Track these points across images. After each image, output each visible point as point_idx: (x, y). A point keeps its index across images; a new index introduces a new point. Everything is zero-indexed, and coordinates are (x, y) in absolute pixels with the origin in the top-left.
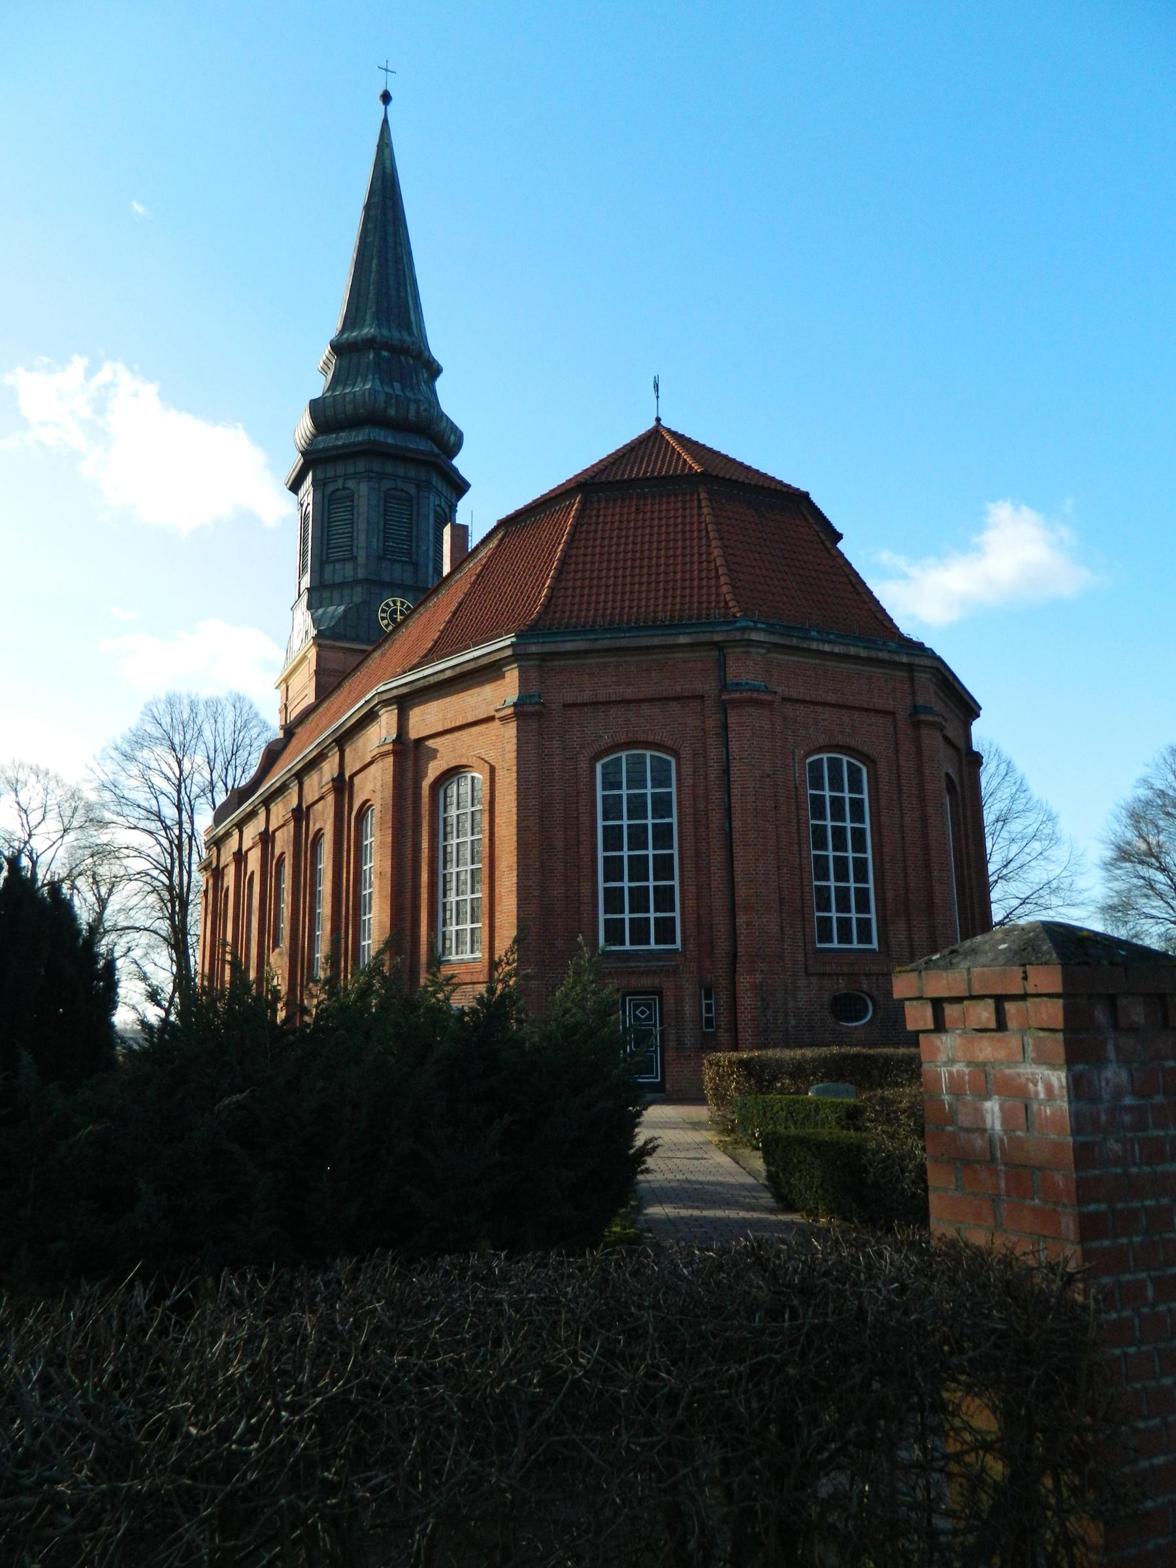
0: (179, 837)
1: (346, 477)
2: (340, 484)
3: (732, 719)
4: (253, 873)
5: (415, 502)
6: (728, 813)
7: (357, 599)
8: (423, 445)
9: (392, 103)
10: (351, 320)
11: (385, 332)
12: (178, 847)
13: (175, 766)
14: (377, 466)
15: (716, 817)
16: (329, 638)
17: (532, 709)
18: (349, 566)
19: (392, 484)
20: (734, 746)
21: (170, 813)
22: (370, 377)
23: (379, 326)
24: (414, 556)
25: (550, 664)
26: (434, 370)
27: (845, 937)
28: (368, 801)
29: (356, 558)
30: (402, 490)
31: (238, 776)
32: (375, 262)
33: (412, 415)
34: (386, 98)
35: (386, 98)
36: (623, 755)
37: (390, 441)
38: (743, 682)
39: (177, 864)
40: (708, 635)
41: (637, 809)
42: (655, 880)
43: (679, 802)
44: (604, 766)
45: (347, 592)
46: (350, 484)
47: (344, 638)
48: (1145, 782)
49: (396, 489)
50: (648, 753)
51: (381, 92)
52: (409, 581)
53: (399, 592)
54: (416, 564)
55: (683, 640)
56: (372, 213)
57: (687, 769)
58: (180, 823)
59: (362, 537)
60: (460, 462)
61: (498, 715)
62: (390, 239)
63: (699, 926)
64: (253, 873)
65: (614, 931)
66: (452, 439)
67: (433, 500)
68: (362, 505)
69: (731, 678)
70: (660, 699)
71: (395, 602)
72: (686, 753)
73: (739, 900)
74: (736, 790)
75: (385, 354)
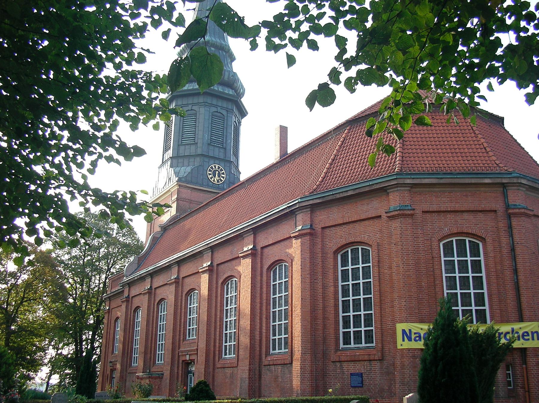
1: (193, 104)
2: (189, 108)
5: (226, 118)
6: (516, 271)
7: (197, 164)
8: (229, 92)
11: (213, 39)
14: (209, 100)
15: (508, 274)
16: (183, 182)
18: (193, 147)
19: (214, 109)
20: (517, 238)
24: (224, 145)
25: (413, 190)
26: (233, 59)
29: (197, 143)
36: (454, 239)
38: (518, 204)
40: (500, 179)
41: (357, 304)
43: (486, 265)
44: (341, 255)
45: (192, 160)
46: (194, 108)
47: (191, 183)
48: (440, 315)
52: (222, 157)
53: (217, 162)
54: (225, 149)
57: (490, 248)
59: (201, 133)
60: (245, 101)
65: (347, 341)
69: (511, 202)
70: (473, 211)
71: (215, 166)
72: (489, 240)
74: (519, 259)
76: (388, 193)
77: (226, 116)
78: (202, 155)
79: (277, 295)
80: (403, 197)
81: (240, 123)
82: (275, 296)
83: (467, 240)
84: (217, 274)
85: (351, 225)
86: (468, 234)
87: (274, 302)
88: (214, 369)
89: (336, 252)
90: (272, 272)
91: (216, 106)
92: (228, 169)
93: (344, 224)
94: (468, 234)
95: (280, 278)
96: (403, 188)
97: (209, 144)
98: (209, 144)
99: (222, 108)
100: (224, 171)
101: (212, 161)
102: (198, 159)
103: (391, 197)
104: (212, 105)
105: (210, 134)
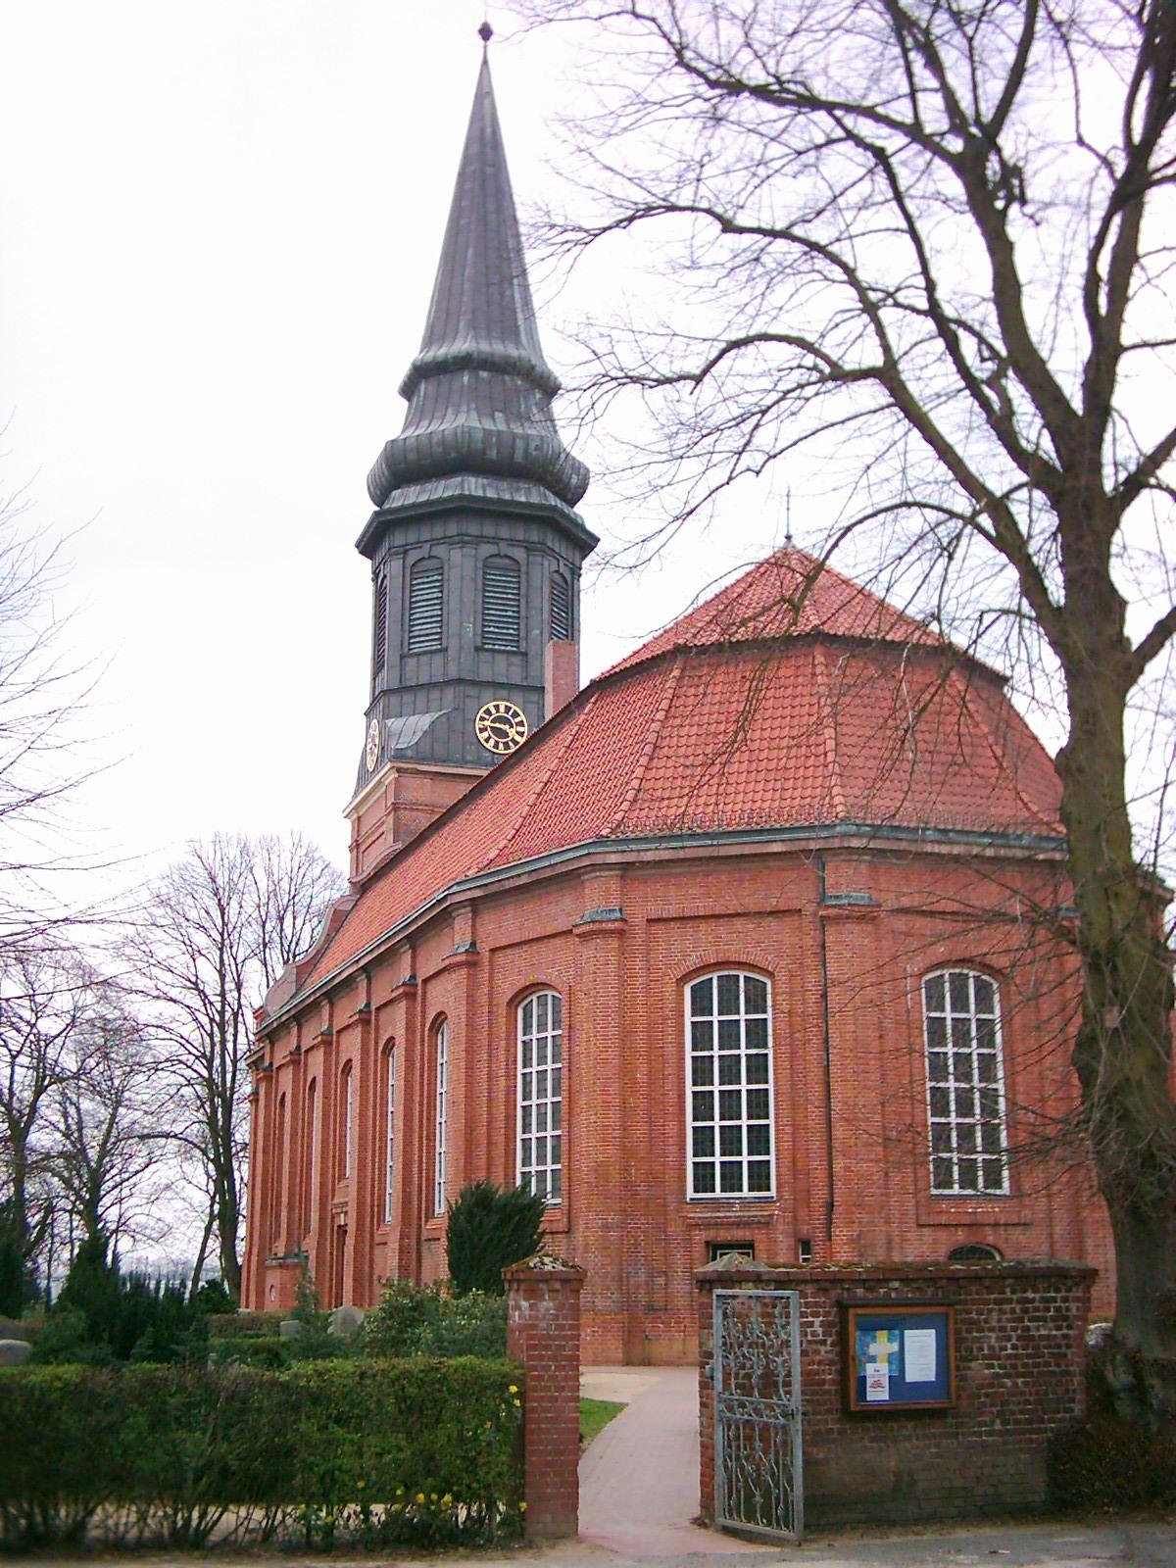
0: (222, 1013)
1: (435, 542)
2: (424, 552)
3: (831, 937)
4: (314, 1079)
5: (523, 569)
9: (493, 39)
10: (438, 328)
12: (222, 1022)
13: (216, 913)
14: (473, 528)
17: (610, 926)
18: (438, 659)
21: (212, 987)
22: (464, 408)
23: (476, 338)
24: (523, 644)
27: (968, 1180)
28: (442, 1013)
29: (446, 650)
30: (506, 556)
31: (298, 928)
32: (470, 252)
33: (519, 457)
34: (486, 33)
35: (486, 33)
37: (491, 494)
39: (218, 1049)
40: (804, 843)
42: (750, 1117)
45: (435, 694)
49: (498, 555)
50: (742, 975)
51: (479, 27)
53: (504, 693)
54: (525, 654)
55: (776, 848)
56: (465, 203)
58: (223, 995)
61: (576, 931)
62: (492, 218)
63: (795, 1168)
64: (314, 1079)
65: (704, 1181)
66: (574, 480)
67: (549, 564)
68: (453, 577)
71: (497, 707)
73: (836, 1144)
75: (484, 374)
76: (583, 882)
77: (523, 562)
78: (460, 681)
79: (535, 1068)
80: (607, 891)
81: (576, 572)
82: (527, 1070)
83: (742, 975)
84: (377, 1030)
85: (535, 946)
86: (741, 965)
87: (527, 1084)
88: (371, 1248)
89: (514, 1002)
90: (520, 1012)
91: (495, 540)
92: (533, 708)
93: (510, 946)
94: (741, 965)
95: (542, 1027)
96: (607, 873)
97: (477, 649)
98: (477, 649)
99: (512, 542)
100: (523, 717)
101: (488, 693)
102: (449, 693)
103: (587, 891)
104: (481, 539)
105: (480, 621)
